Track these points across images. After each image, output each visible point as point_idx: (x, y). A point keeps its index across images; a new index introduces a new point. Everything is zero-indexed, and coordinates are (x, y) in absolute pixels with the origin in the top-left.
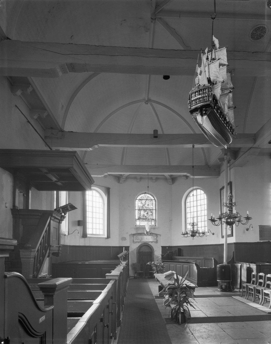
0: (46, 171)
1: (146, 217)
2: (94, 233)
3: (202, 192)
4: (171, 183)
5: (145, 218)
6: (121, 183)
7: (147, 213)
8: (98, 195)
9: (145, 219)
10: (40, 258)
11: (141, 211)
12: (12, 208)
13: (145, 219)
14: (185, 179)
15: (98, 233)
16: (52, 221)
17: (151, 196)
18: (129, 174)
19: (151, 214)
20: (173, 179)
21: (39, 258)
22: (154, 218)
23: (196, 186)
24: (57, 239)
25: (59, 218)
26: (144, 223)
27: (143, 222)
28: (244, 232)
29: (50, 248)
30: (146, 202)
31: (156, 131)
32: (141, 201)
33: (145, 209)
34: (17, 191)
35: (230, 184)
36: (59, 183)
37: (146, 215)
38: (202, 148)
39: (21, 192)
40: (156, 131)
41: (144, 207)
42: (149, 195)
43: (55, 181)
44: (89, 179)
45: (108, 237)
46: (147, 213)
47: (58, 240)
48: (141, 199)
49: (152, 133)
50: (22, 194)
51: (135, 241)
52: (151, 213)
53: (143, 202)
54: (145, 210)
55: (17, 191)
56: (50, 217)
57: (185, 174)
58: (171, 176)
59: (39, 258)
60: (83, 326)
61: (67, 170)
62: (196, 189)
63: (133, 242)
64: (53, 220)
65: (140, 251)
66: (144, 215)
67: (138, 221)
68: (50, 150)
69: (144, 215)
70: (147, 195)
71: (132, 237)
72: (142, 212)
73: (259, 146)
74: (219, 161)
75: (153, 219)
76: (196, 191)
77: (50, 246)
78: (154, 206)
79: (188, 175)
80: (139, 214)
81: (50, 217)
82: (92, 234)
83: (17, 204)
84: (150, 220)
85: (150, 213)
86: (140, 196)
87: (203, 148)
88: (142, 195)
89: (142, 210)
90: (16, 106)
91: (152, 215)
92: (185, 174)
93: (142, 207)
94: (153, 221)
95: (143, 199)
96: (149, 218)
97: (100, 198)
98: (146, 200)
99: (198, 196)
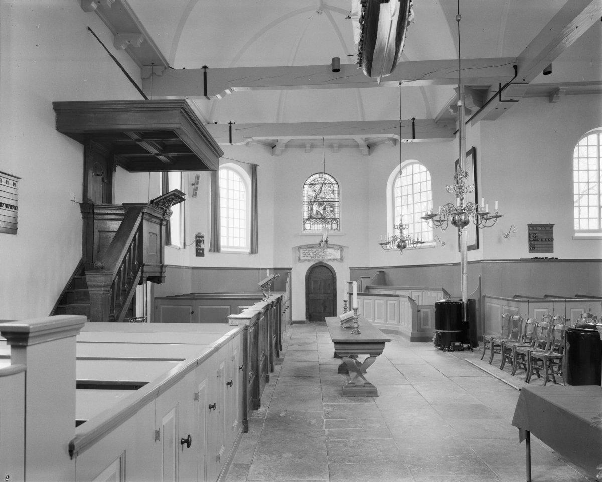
0: (136, 137)
1: (321, 214)
2: (231, 244)
3: (424, 168)
4: (367, 154)
5: (320, 217)
6: (278, 156)
7: (325, 209)
8: (237, 177)
9: (319, 219)
10: (124, 286)
11: (313, 205)
12: (82, 202)
13: (319, 219)
14: (393, 145)
15: (236, 245)
16: (145, 223)
17: (330, 178)
18: (290, 139)
19: (332, 209)
20: (370, 147)
21: (121, 286)
22: (336, 217)
23: (413, 159)
24: (156, 253)
25: (160, 216)
26: (318, 225)
27: (316, 225)
28: (499, 241)
29: (143, 269)
30: (321, 188)
31: (336, 60)
32: (312, 187)
33: (321, 200)
34: (91, 173)
35: (473, 152)
36: (161, 158)
37: (321, 212)
38: (421, 88)
39: (98, 175)
40: (336, 60)
41: (319, 198)
42: (327, 176)
43: (155, 154)
44: (212, 146)
45: (254, 249)
46: (325, 209)
47: (159, 254)
48: (313, 182)
49: (330, 62)
50: (100, 178)
51: (302, 258)
52: (331, 207)
53: (317, 187)
54: (320, 204)
55: (91, 173)
56: (141, 214)
57: (391, 136)
58: (367, 140)
59: (121, 286)
60: (37, 324)
61: (171, 134)
62: (412, 164)
63: (300, 259)
64: (148, 220)
65: (479, 342)
66: (317, 212)
67: (308, 222)
68: (144, 99)
69: (317, 212)
70: (324, 175)
71: (298, 252)
72: (315, 207)
73: (524, 80)
74: (451, 110)
75: (334, 219)
76: (413, 166)
77: (143, 265)
78: (336, 194)
79: (397, 137)
80: (309, 209)
81: (141, 214)
82: (228, 247)
83: (90, 194)
84: (329, 220)
85: (329, 209)
86: (312, 178)
87: (422, 86)
88: (314, 176)
89: (315, 203)
90: (89, 28)
91: (333, 211)
92: (391, 136)
93: (315, 197)
94: (334, 222)
95: (317, 182)
96: (328, 217)
97: (241, 183)
98: (322, 184)
99: (415, 176)
